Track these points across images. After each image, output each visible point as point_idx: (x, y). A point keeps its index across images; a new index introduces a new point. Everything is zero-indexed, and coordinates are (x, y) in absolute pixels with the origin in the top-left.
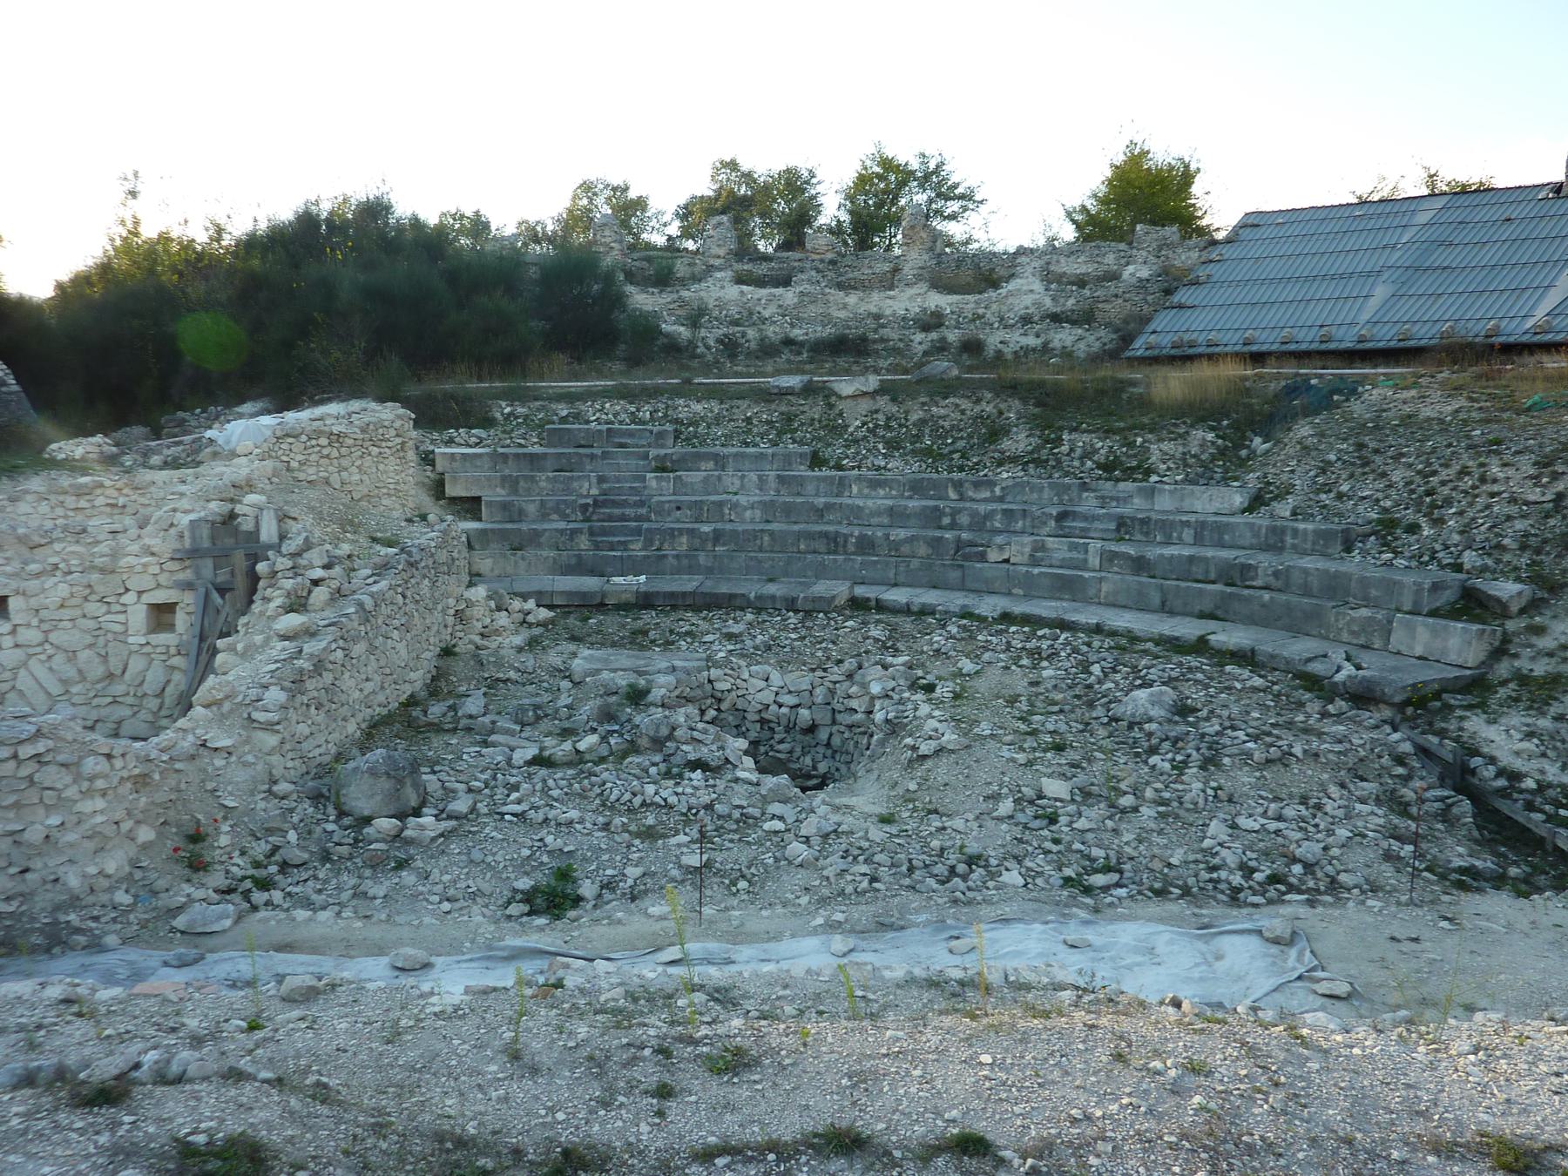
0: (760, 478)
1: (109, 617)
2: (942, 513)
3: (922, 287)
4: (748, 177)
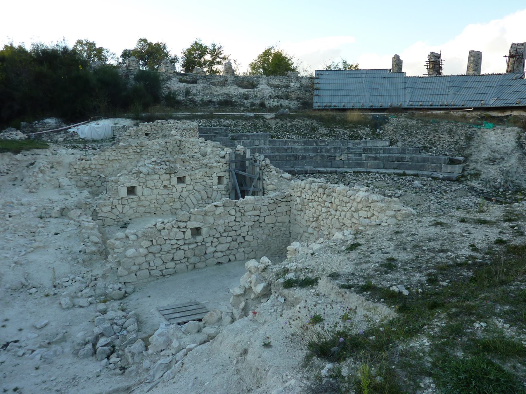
2: (318, 149)
3: (235, 87)
4: (150, 44)
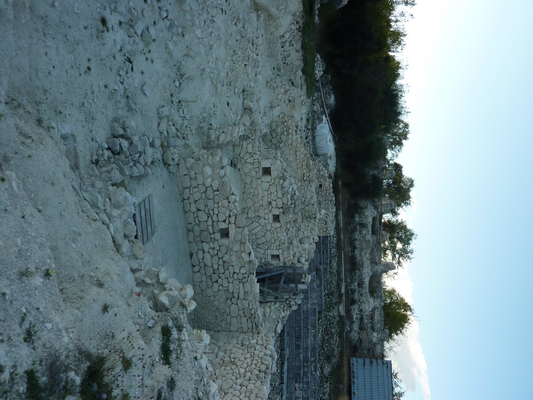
0: (315, 304)
1: (275, 246)
2: (307, 363)
3: (371, 274)
4: (408, 190)
